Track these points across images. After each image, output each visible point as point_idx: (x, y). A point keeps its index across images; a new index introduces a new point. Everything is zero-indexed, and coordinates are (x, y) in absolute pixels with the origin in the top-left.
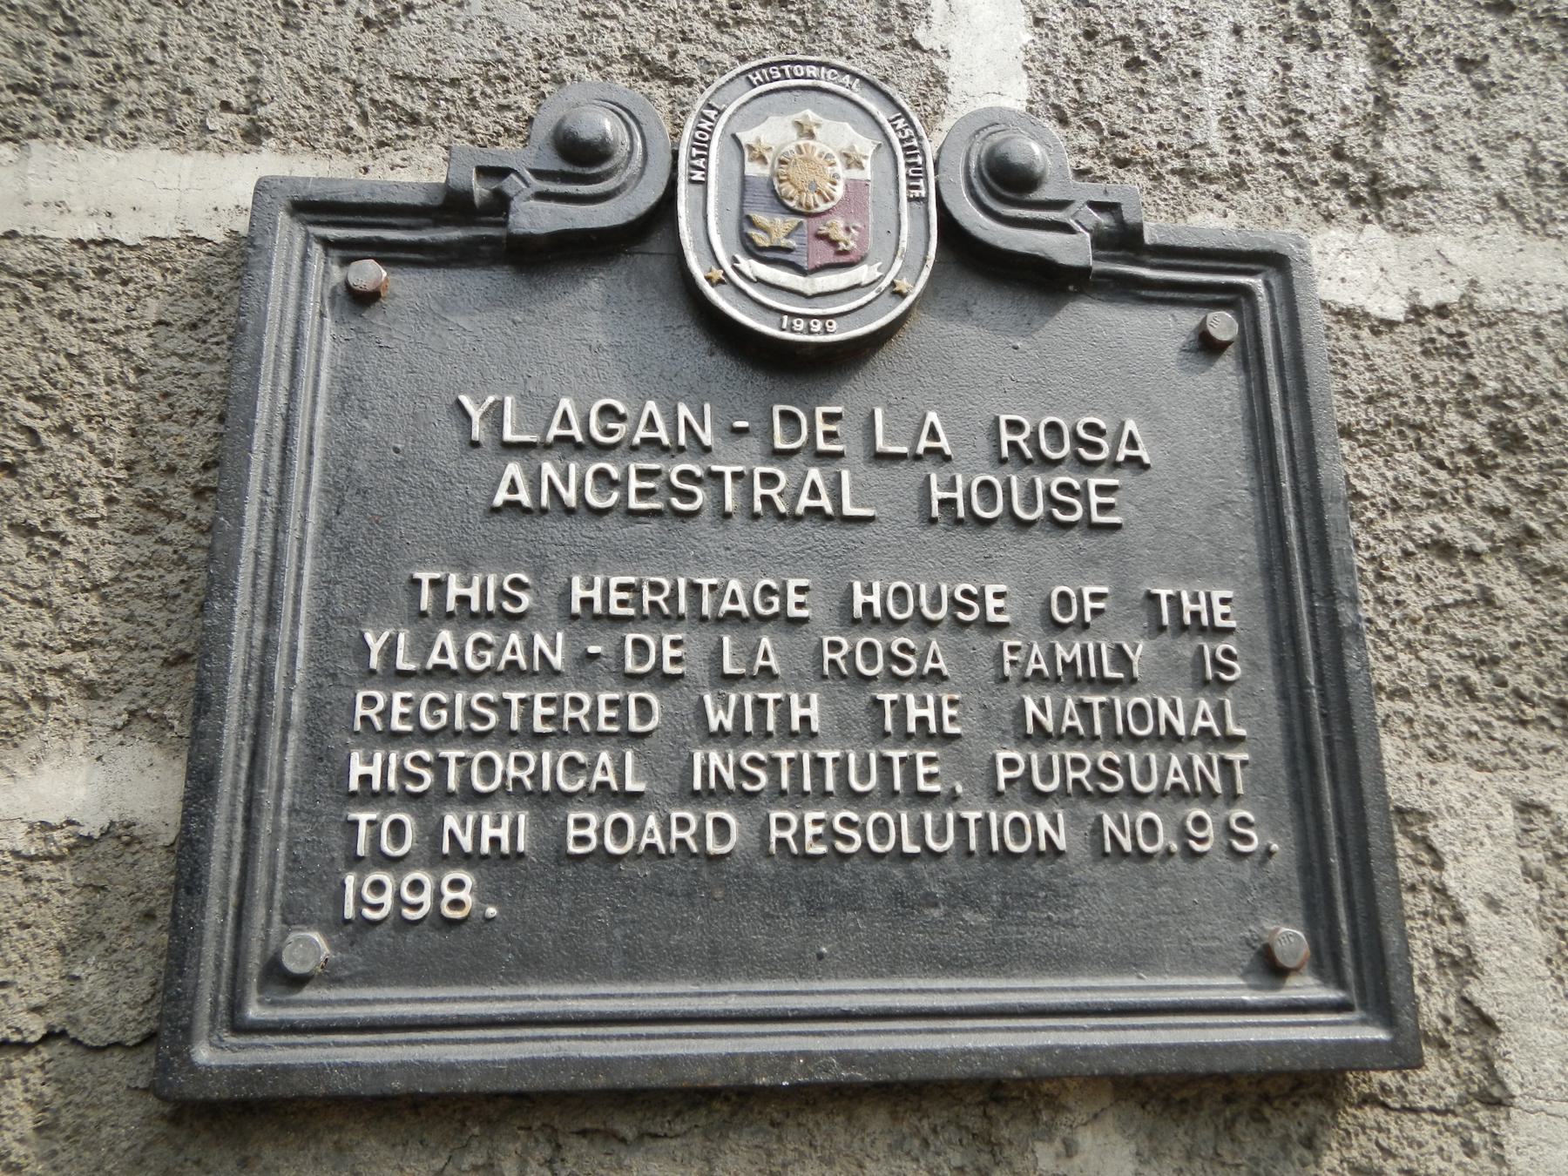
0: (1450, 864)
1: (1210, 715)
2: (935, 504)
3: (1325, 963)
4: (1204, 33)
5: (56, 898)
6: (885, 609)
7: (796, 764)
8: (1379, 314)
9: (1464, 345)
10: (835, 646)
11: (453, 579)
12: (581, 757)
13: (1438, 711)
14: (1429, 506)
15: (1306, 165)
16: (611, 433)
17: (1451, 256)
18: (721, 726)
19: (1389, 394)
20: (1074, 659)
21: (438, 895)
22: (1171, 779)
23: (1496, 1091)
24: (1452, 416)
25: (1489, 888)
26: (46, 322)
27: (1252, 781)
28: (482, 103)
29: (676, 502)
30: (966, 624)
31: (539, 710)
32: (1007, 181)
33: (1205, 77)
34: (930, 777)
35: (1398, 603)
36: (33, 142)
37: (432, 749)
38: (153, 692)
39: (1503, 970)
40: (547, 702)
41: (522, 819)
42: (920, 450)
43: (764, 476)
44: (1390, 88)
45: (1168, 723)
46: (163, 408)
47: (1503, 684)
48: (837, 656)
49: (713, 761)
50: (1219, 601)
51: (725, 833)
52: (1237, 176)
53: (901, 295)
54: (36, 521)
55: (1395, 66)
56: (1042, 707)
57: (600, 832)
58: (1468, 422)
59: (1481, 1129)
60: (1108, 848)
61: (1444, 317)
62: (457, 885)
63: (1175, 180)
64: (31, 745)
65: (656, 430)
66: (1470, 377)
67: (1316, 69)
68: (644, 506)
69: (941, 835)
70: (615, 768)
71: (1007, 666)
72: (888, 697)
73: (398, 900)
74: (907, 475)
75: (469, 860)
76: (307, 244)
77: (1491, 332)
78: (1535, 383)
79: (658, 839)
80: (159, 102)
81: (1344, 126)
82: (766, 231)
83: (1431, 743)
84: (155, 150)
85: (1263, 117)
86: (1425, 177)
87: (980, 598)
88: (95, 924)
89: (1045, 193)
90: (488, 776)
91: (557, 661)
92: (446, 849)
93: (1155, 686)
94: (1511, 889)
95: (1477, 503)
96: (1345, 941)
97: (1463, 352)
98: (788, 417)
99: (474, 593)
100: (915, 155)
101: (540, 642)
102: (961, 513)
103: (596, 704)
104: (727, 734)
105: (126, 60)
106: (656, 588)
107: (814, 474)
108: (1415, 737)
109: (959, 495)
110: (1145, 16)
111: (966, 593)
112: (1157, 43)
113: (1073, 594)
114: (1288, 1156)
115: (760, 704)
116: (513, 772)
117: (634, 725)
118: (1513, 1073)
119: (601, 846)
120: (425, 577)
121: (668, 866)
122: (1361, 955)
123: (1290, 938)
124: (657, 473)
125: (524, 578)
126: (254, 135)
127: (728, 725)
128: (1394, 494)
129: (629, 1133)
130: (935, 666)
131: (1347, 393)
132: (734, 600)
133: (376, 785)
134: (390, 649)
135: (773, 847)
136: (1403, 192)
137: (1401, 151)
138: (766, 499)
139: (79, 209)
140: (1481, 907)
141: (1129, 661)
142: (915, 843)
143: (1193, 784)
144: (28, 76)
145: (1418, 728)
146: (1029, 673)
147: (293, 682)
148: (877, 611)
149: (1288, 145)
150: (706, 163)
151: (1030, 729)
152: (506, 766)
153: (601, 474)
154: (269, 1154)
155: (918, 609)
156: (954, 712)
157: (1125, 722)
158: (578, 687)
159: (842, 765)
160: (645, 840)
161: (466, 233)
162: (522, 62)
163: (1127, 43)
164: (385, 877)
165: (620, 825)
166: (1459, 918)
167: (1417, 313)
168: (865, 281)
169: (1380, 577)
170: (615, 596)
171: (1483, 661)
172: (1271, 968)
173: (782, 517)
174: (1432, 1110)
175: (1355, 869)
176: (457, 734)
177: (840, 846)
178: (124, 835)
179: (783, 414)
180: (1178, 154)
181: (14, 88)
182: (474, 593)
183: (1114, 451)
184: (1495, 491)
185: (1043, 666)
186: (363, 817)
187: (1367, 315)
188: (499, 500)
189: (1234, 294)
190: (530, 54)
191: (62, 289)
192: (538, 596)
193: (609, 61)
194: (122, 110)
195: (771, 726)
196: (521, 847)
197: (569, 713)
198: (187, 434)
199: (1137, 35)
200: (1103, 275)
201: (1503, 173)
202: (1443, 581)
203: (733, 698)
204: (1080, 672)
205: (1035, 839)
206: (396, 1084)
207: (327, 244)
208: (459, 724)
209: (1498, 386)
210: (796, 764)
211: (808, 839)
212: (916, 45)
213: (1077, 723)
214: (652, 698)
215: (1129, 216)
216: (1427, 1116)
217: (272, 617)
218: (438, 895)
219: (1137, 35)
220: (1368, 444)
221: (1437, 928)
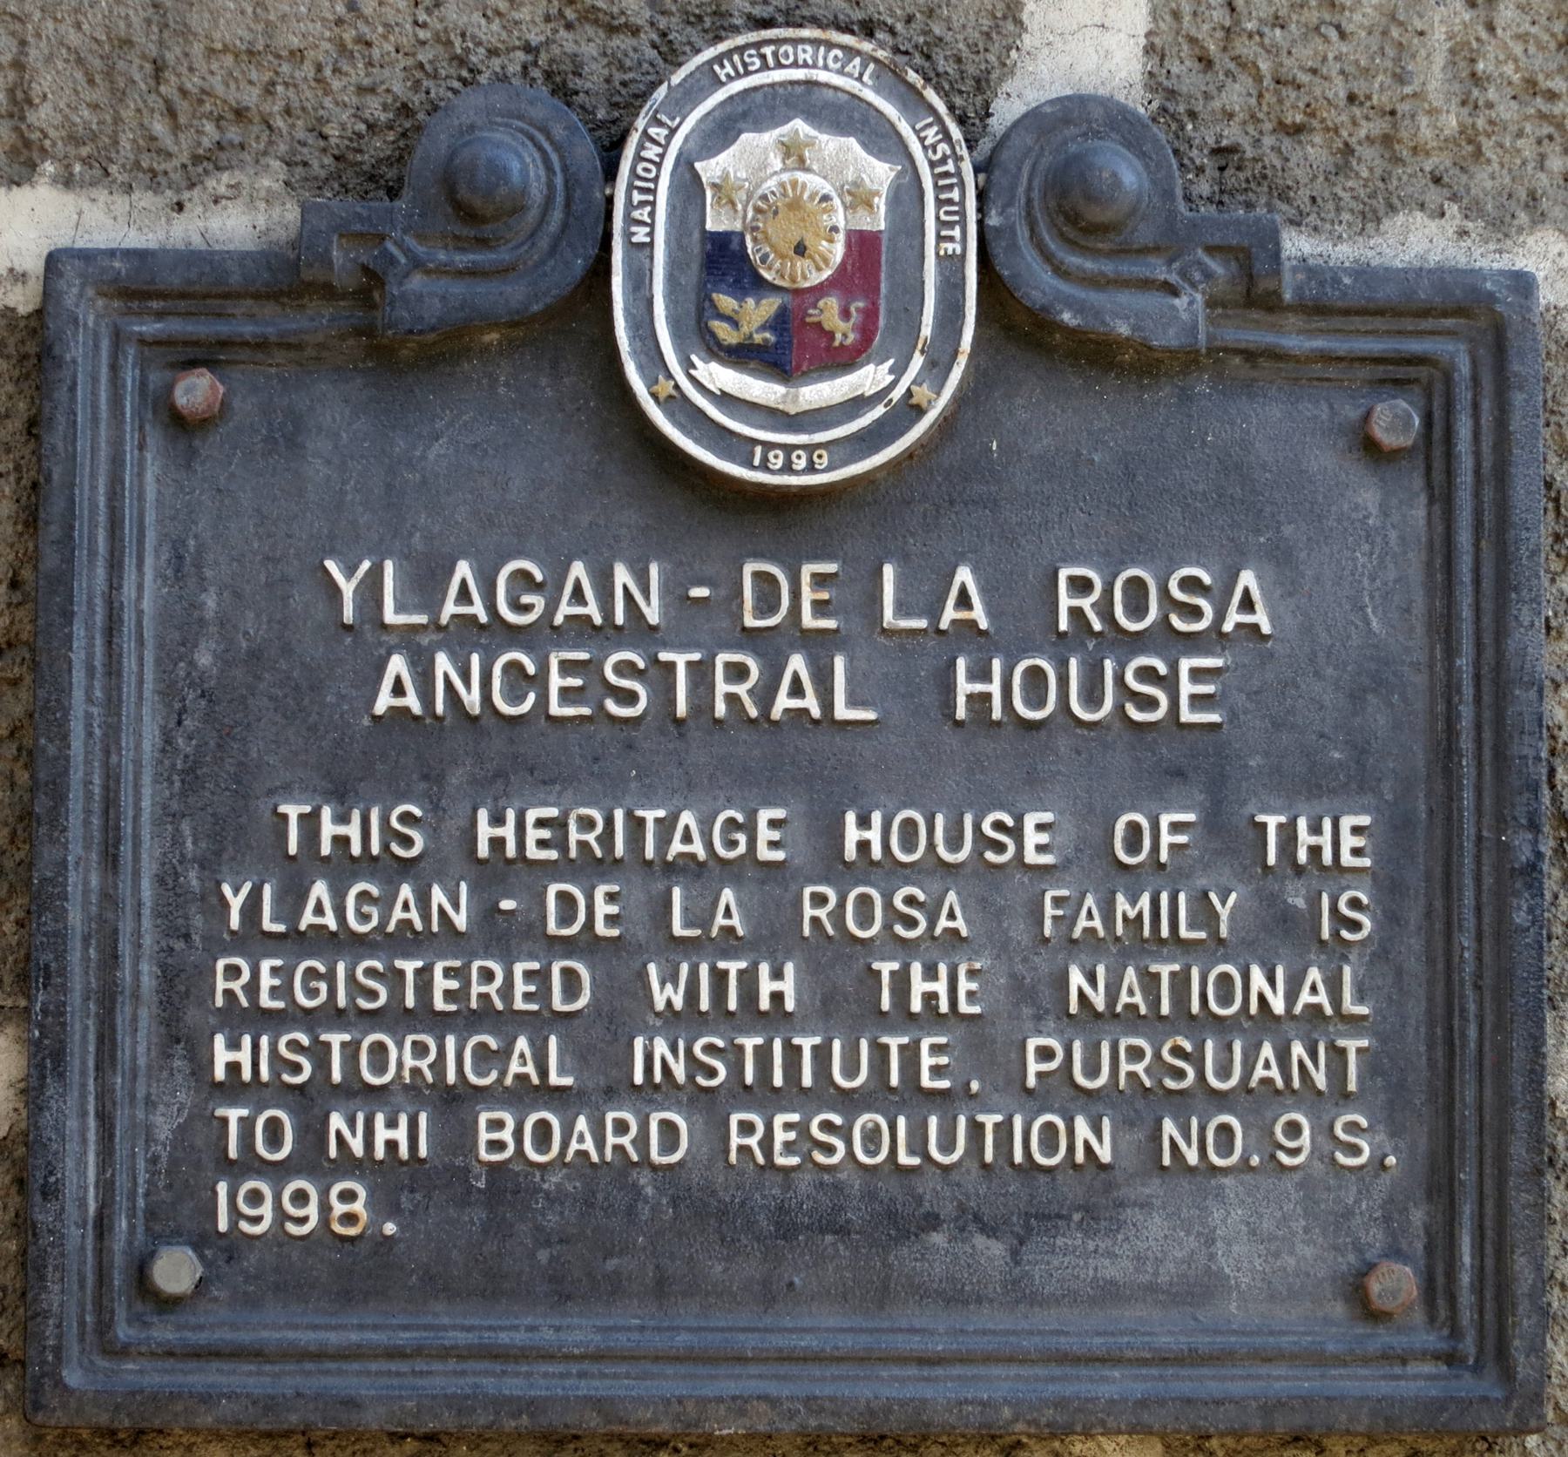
1: (1321, 987)
7: (763, 1054)
16: (528, 608)
18: (669, 1003)
20: (1140, 915)
21: (325, 1208)
22: (1259, 1072)
28: (336, 84)
29: (612, 706)
31: (441, 983)
34: (937, 1071)
37: (311, 1030)
41: (423, 1119)
42: (944, 625)
45: (1261, 997)
48: (822, 913)
49: (650, 1053)
50: (1347, 836)
51: (661, 1137)
56: (1092, 979)
57: (518, 1134)
60: (1167, 1161)
65: (585, 604)
68: (570, 711)
69: (947, 1145)
70: (534, 1055)
71: (1048, 923)
73: (281, 1216)
79: (589, 1145)
82: (735, 324)
85: (1523, 38)
90: (379, 1066)
91: (461, 920)
96: (1465, 1278)
100: (950, 187)
101: (438, 896)
102: (997, 714)
104: (676, 1014)
106: (587, 824)
109: (995, 688)
113: (1145, 824)
115: (720, 977)
116: (409, 1062)
117: (558, 1004)
127: (678, 1003)
130: (951, 924)
133: (247, 1074)
134: (252, 909)
135: (733, 1157)
138: (732, 699)
142: (911, 1152)
143: (1287, 1078)
146: (1077, 933)
147: (140, 946)
148: (877, 852)
150: (652, 214)
151: (1074, 1007)
152: (403, 1058)
153: (514, 668)
156: (974, 986)
158: (487, 955)
159: (822, 1055)
165: (543, 1129)
168: (869, 391)
170: (533, 834)
177: (820, 1157)
183: (1220, 616)
186: (234, 1114)
188: (381, 707)
192: (433, 833)
195: (732, 1005)
203: (685, 968)
204: (1146, 932)
205: (1071, 1148)
210: (763, 1054)
211: (778, 1147)
213: (1138, 999)
217: (111, 860)
218: (325, 1208)
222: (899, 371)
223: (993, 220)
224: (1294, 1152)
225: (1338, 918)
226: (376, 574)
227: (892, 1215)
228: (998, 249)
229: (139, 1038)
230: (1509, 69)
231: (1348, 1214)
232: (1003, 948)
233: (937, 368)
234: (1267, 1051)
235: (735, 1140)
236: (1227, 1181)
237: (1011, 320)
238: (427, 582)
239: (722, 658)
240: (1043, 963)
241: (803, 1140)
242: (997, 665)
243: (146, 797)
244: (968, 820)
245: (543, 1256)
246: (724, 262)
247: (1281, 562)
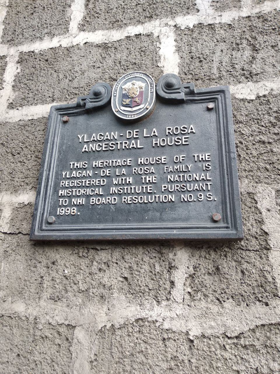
0: (259, 203)
2: (154, 144)
4: (215, 53)
5: (21, 213)
6: (144, 162)
7: (127, 189)
8: (249, 99)
9: (269, 102)
10: (135, 169)
11: (76, 163)
12: (93, 189)
13: (259, 174)
14: (259, 134)
15: (235, 73)
16: (101, 138)
17: (267, 85)
19: (251, 114)
21: (71, 211)
23: (268, 247)
24: (266, 116)
25: (268, 207)
26: (24, 132)
27: (211, 188)
30: (158, 164)
31: (87, 182)
33: (214, 61)
35: (251, 154)
36: (24, 107)
37: (72, 189)
38: (35, 184)
39: (270, 223)
40: (89, 181)
41: (84, 199)
43: (125, 143)
44: (255, 55)
45: (195, 178)
46: (39, 143)
47: (275, 167)
49: (113, 189)
51: (112, 200)
52: (220, 78)
53: (147, 109)
54: (22, 161)
55: (256, 50)
57: (96, 200)
58: (269, 117)
59: (264, 254)
60: (182, 200)
61: (264, 97)
62: (74, 209)
63: (207, 81)
64: (19, 192)
66: (270, 108)
67: (239, 54)
72: (143, 177)
74: (149, 140)
75: (75, 205)
76: (58, 115)
77: (276, 99)
80: (41, 98)
81: (244, 64)
82: (125, 102)
83: (257, 180)
84: (39, 105)
85: (226, 66)
86: (262, 70)
87: (161, 159)
88: (26, 217)
89: (177, 87)
91: (90, 175)
92: (72, 204)
93: (194, 172)
94: (273, 207)
95: (271, 133)
97: (269, 103)
98: (130, 132)
99: (79, 165)
101: (88, 172)
103: (96, 181)
105: (36, 92)
106: (107, 162)
107: (133, 141)
108: (254, 179)
109: (158, 142)
110: (203, 52)
111: (159, 159)
112: (205, 57)
114: (221, 258)
119: (96, 203)
120: (72, 163)
121: (106, 206)
122: (231, 217)
124: (108, 144)
125: (86, 162)
126: (53, 101)
127: (117, 183)
128: (252, 133)
129: (99, 248)
131: (242, 115)
132: (119, 163)
136: (257, 75)
137: (256, 67)
138: (125, 146)
139: (29, 115)
140: (266, 211)
141: (188, 168)
143: (199, 188)
144: (23, 97)
145: (254, 178)
149: (232, 70)
152: (82, 191)
153: (99, 145)
154: (47, 250)
155: (150, 162)
157: (187, 178)
160: (102, 202)
161: (82, 110)
162: (92, 82)
163: (199, 58)
164: (63, 208)
165: (99, 199)
166: (261, 213)
167: (258, 97)
169: (247, 149)
170: (100, 164)
171: (270, 164)
173: (128, 149)
174: (253, 250)
175: (231, 202)
176: (75, 187)
179: (129, 132)
180: (208, 76)
181: (22, 99)
182: (79, 165)
183: (188, 131)
185: (172, 170)
186: (61, 200)
187: (247, 99)
190: (94, 81)
191: (27, 127)
193: (106, 79)
194: (35, 100)
196: (83, 203)
197: (92, 183)
198: (42, 146)
199: (201, 56)
200: (188, 100)
202: (262, 149)
203: (118, 179)
205: (168, 199)
206: (62, 238)
207: (60, 114)
208: (75, 185)
209: (277, 109)
210: (127, 189)
212: (158, 66)
213: (178, 179)
214: (105, 180)
215: (191, 89)
216: (252, 252)
218: (71, 211)
219: (201, 56)
220: (246, 124)
221: (256, 215)
222: (145, 105)
223: (157, 88)
224: (201, 199)
225: (206, 167)
226: (84, 136)
227: (144, 210)
228: (158, 91)
229: (50, 191)
230: (225, 70)
231: (210, 207)
232: (159, 174)
233: (150, 104)
234: (196, 185)
235: (123, 200)
236: (191, 203)
238: (90, 137)
239: (124, 142)
240: (165, 176)
241: (132, 199)
242: (158, 139)
244: (155, 158)
245: (98, 217)
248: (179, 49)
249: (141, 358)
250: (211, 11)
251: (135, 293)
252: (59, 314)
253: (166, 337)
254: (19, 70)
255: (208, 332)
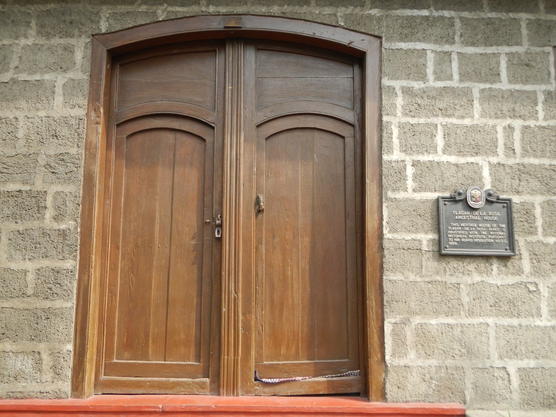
3: (510, 250)
32: (490, 195)
49: (470, 236)
50: (504, 226)
51: (471, 240)
67: (513, 181)
78: (529, 208)
118: (523, 257)
122: (512, 249)
123: (508, 248)
137: (520, 189)
172: (506, 250)
178: (434, 239)
184: (525, 217)
189: (508, 204)
201: (529, 190)
237: (487, 201)
243: (444, 223)
246: (472, 197)
247: (499, 212)
248: (491, 174)
249: (483, 292)
250: (503, 156)
251: (481, 273)
252: (454, 280)
253: (491, 285)
254: (414, 171)
255: (503, 284)
